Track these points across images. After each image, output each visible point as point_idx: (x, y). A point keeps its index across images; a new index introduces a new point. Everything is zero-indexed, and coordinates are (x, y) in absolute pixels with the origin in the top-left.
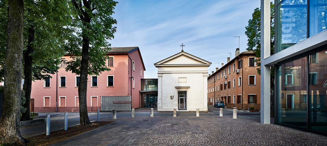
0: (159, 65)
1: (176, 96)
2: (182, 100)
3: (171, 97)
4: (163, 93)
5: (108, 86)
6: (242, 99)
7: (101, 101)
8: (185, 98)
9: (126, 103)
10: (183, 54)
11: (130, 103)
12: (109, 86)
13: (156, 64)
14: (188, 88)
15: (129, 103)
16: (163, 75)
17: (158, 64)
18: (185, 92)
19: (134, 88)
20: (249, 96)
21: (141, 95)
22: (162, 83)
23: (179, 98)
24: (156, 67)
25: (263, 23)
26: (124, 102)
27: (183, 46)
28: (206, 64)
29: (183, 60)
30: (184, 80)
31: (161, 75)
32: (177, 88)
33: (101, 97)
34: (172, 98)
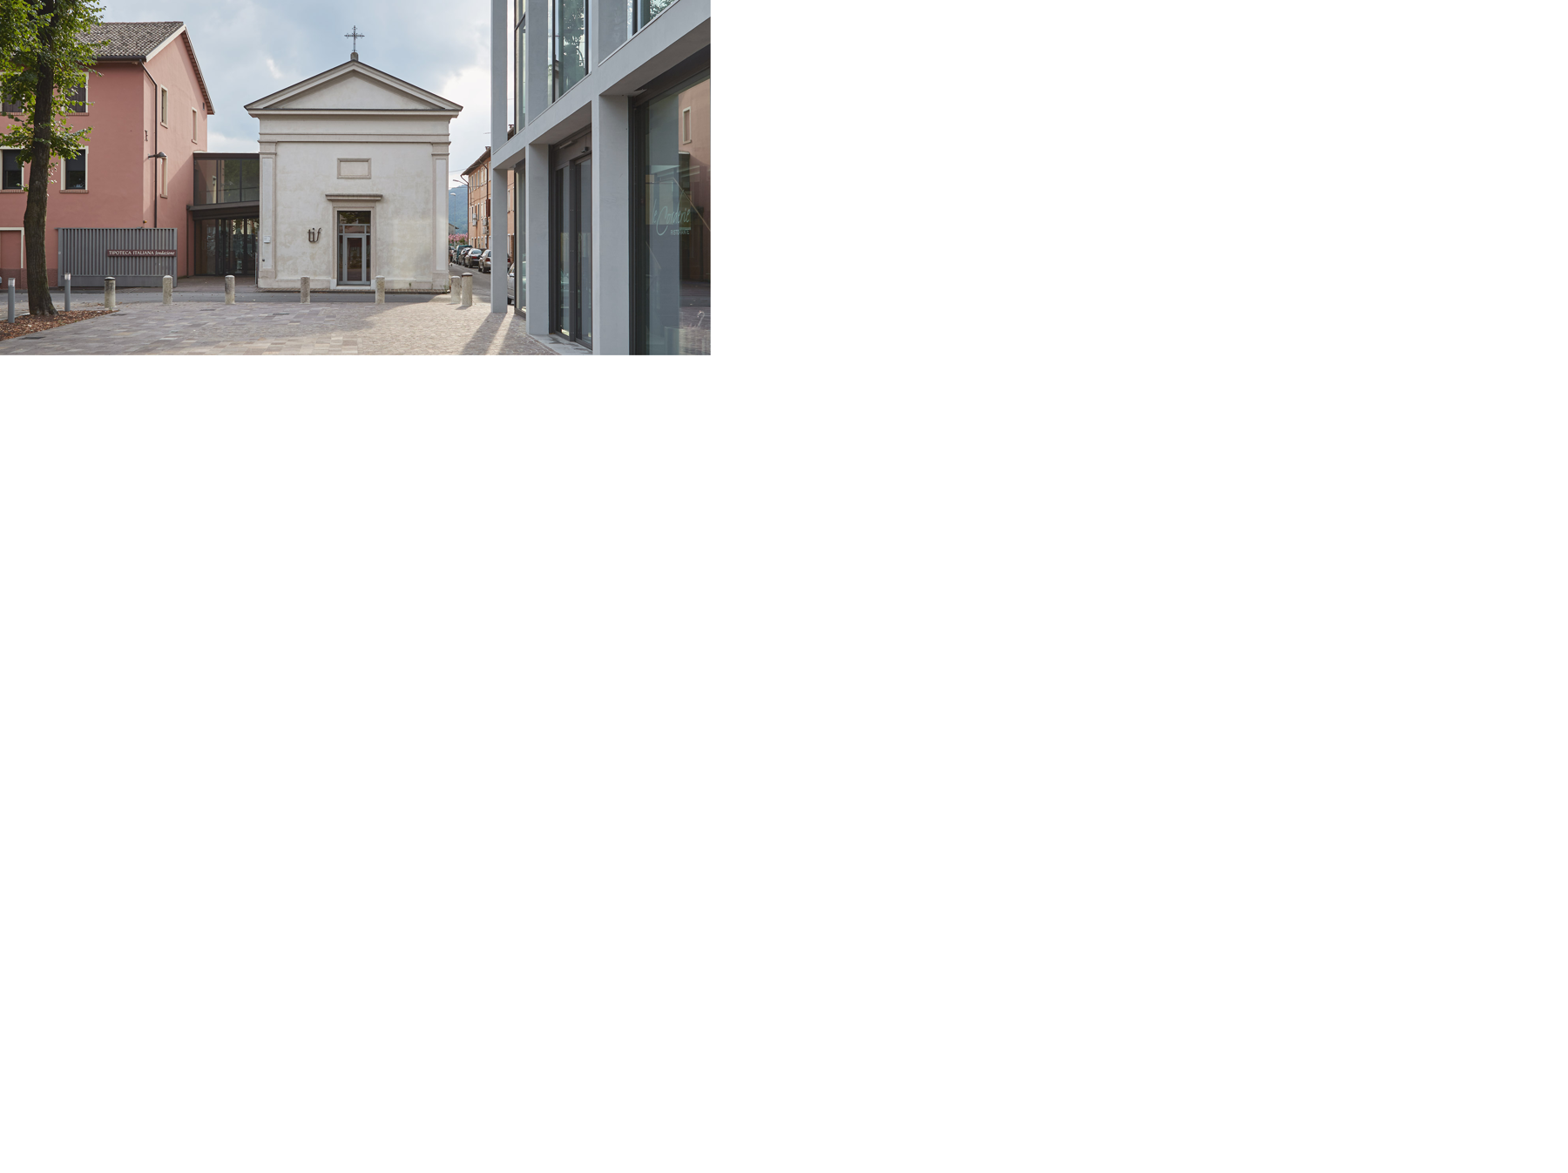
0: (265, 109)
1: (331, 232)
2: (355, 244)
3: (309, 232)
4: (279, 220)
5: (63, 187)
6: (199, 351)
7: (61, 247)
8: (368, 238)
9: (158, 256)
10: (354, 71)
11: (173, 257)
12: (67, 188)
13: (254, 106)
14: (377, 199)
15: (169, 256)
16: (281, 149)
17: (261, 107)
18: (365, 217)
19: (166, 194)
20: (339, 177)
21: (195, 221)
22: (275, 179)
23: (340, 239)
24: (253, 116)
25: (589, 234)
26: (150, 250)
27: (355, 36)
28: (443, 109)
29: (355, 95)
30: (360, 169)
31: (271, 149)
32: (332, 199)
33: (60, 232)
34: (313, 237)
